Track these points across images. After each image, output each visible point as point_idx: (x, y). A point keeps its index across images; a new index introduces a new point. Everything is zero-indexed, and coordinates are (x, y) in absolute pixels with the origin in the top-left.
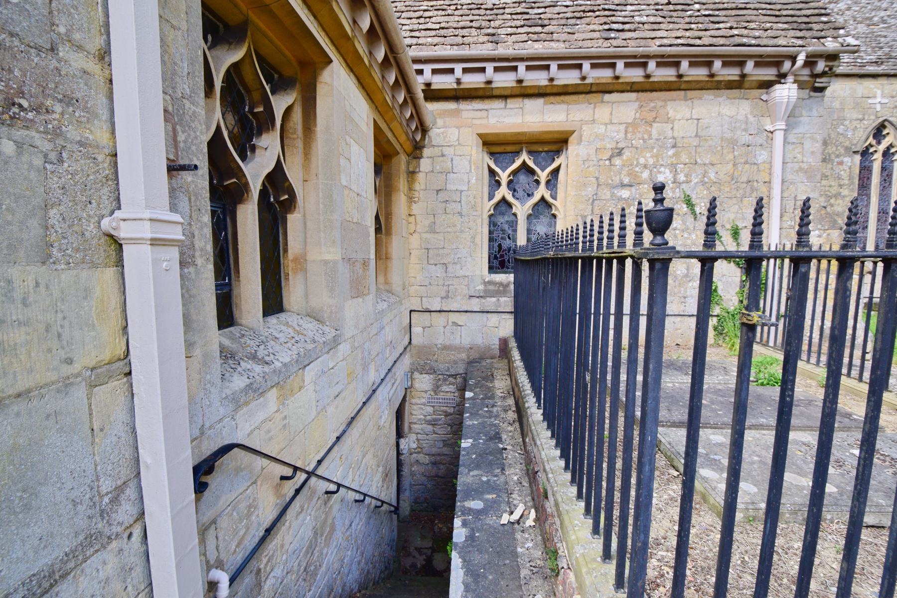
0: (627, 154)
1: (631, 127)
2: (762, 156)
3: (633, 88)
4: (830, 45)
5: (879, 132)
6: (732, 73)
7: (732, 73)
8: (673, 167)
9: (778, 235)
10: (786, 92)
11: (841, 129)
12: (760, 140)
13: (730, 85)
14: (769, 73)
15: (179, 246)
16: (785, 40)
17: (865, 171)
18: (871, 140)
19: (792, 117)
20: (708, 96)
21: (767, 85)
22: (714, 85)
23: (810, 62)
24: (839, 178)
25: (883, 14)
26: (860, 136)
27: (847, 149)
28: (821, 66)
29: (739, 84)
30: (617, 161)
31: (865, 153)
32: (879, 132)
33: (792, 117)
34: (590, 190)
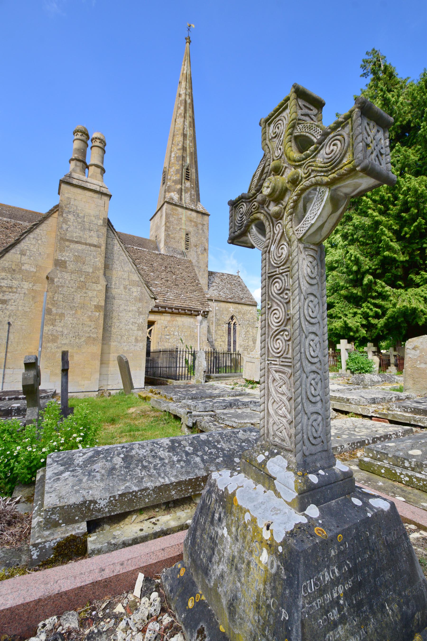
0: (168, 328)
1: (169, 321)
2: (196, 331)
3: (169, 313)
4: (207, 310)
5: (232, 318)
6: (189, 313)
7: (189, 313)
8: (178, 331)
9: (182, 350)
10: (200, 318)
11: (223, 316)
12: (195, 327)
13: (189, 315)
14: (196, 313)
15: (229, 350)
16: (199, 308)
17: (229, 329)
18: (230, 320)
19: (201, 323)
20: (185, 316)
21: (196, 315)
22: (186, 314)
23: (204, 312)
24: (223, 330)
25: (234, 282)
26: (227, 319)
27: (225, 322)
28: (206, 313)
29: (191, 315)
30: (166, 329)
31: (229, 324)
32: (232, 318)
33: (201, 323)
34: (160, 336)
